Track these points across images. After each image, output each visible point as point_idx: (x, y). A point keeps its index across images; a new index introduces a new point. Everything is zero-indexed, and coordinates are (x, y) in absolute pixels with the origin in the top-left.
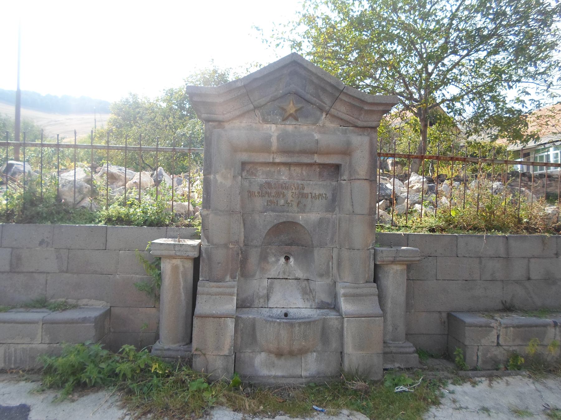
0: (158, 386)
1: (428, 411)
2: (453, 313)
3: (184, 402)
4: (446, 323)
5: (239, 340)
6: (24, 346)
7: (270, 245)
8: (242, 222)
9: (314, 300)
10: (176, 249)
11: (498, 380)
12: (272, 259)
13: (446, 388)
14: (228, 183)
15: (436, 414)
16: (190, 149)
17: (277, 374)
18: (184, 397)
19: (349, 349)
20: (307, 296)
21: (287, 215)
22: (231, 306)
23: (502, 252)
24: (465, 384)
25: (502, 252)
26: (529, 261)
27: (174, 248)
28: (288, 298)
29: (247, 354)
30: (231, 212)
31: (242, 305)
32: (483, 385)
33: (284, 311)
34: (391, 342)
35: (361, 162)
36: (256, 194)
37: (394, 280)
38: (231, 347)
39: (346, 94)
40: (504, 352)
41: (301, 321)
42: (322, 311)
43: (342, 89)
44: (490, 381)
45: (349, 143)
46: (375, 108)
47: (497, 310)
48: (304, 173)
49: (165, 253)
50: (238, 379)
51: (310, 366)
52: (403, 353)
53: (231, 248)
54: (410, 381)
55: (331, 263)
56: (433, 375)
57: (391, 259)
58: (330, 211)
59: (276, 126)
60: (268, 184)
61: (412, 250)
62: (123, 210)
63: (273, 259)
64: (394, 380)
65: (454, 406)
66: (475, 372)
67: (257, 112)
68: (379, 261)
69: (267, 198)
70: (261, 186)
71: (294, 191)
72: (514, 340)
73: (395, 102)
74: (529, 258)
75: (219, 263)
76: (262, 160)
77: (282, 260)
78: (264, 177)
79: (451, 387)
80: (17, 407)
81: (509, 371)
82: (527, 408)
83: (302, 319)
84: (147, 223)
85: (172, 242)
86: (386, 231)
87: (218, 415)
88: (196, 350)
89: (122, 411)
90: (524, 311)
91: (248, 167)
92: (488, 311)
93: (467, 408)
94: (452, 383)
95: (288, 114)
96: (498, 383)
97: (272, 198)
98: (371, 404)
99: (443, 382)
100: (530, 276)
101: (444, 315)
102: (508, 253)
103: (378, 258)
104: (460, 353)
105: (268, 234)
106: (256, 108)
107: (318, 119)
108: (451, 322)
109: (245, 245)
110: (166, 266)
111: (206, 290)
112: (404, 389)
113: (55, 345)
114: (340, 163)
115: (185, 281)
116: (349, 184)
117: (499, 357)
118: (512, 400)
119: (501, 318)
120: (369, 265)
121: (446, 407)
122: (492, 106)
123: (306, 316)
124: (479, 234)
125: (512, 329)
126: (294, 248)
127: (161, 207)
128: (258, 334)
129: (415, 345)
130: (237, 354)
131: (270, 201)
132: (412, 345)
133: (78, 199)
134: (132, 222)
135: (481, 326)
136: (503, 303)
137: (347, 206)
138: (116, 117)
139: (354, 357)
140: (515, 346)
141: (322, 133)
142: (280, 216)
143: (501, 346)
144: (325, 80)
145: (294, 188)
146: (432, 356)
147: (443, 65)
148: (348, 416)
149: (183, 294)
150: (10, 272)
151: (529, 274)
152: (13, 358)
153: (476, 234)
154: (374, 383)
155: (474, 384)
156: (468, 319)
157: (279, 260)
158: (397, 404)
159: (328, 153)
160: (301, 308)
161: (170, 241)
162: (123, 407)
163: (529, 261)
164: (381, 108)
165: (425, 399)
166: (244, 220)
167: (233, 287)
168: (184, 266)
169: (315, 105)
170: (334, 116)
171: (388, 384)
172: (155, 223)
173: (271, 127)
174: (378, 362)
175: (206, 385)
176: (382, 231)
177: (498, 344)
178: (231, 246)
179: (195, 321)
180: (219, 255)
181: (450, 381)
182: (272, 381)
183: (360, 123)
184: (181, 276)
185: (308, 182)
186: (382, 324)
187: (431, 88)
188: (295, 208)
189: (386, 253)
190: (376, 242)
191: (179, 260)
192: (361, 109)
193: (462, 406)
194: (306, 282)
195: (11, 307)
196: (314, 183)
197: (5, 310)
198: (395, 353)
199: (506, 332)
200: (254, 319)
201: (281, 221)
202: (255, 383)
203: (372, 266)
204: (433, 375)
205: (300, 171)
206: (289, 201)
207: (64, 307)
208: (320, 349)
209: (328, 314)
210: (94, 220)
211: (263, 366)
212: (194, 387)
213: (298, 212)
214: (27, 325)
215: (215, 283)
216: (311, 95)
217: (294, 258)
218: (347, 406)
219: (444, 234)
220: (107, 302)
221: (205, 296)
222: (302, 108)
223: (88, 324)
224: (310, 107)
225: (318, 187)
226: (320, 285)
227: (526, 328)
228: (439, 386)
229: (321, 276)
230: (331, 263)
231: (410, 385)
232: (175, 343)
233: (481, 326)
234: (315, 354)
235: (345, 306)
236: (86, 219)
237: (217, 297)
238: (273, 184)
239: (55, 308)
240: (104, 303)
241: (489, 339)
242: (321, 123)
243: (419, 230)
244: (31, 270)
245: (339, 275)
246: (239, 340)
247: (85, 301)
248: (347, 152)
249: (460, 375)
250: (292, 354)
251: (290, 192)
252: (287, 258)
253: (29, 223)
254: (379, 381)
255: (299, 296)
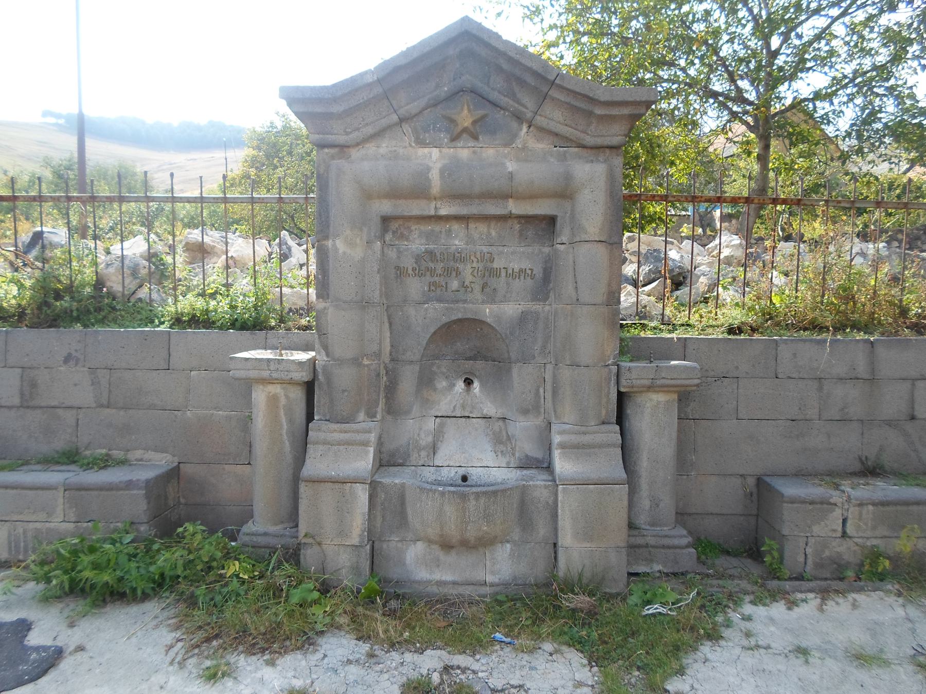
0: (238, 595)
1: (696, 649)
2: (768, 479)
3: (275, 622)
4: (755, 495)
5: (379, 519)
6: (38, 525)
7: (438, 358)
8: (386, 320)
9: (513, 455)
10: (272, 368)
11: (837, 599)
12: (442, 384)
13: (739, 610)
14: (358, 253)
15: (709, 656)
16: (306, 198)
17: (443, 578)
18: (276, 615)
19: (566, 538)
20: (502, 447)
21: (465, 308)
22: (364, 463)
23: (862, 369)
24: (775, 604)
25: (862, 369)
26: (913, 385)
27: (268, 366)
28: (467, 444)
29: (392, 544)
30: (363, 304)
31: (387, 460)
32: (809, 607)
33: (461, 471)
34: (648, 527)
35: (592, 210)
36: (410, 271)
37: (653, 420)
38: (363, 532)
39: (561, 88)
40: (856, 548)
41: (479, 489)
42: (525, 472)
43: (552, 78)
44: (823, 599)
45: (568, 177)
46: (615, 111)
47: (851, 474)
48: (493, 233)
49: (253, 374)
50: (373, 584)
51: (501, 566)
52: (669, 547)
53: (367, 366)
54: (672, 597)
55: (541, 390)
56: (719, 586)
57: (647, 382)
58: (539, 300)
59: (440, 152)
60: (431, 254)
61: (685, 367)
62: (200, 304)
63: (444, 384)
64: (645, 593)
65: (745, 643)
66: (797, 583)
67: (406, 127)
68: (624, 387)
69: (428, 278)
70: (418, 258)
71: (475, 265)
72: (874, 528)
73: (652, 99)
74: (914, 380)
75: (344, 391)
76: (416, 212)
77: (460, 385)
78: (423, 241)
79: (748, 609)
80: (12, 623)
81: (862, 583)
82: (881, 651)
83: (492, 485)
84: (238, 324)
85: (271, 357)
86: (649, 334)
87: (328, 646)
88: (306, 536)
89: (174, 634)
90: (899, 475)
91: (394, 225)
92: (833, 476)
93: (768, 647)
94: (751, 602)
95: (460, 128)
96: (837, 603)
97: (436, 279)
98: (595, 635)
99: (734, 599)
100: (916, 413)
101: (751, 481)
102: (873, 371)
103: (623, 382)
104: (773, 549)
105: (430, 341)
106: (402, 120)
107: (515, 136)
108: (762, 494)
109: (392, 360)
110: (260, 396)
111: (322, 436)
112: (661, 610)
113: (86, 524)
114: (554, 213)
115: (291, 421)
116: (571, 250)
117: (846, 557)
118: (858, 637)
119: (852, 488)
120: (609, 393)
121: (731, 644)
122: (890, 106)
123: (499, 480)
124: (819, 338)
125: (871, 507)
126: (480, 364)
127: (261, 297)
128: (409, 511)
129: (690, 533)
130: (376, 543)
131: (434, 284)
132: (685, 532)
133: (133, 287)
134: (214, 323)
135: (812, 503)
136: (860, 459)
137: (568, 290)
138: (255, 152)
139: (576, 552)
140: (876, 537)
141: (519, 160)
142: (452, 309)
143: (850, 537)
144: (521, 64)
145: (475, 260)
146: (728, 553)
147: (799, 37)
148: (551, 655)
149: (287, 443)
150: (21, 406)
151: (913, 408)
152: (22, 544)
153: (815, 337)
154: (609, 597)
155: (792, 604)
156: (790, 489)
157: (454, 385)
158: (641, 638)
159: (532, 196)
160: (490, 466)
161: (267, 354)
162: (177, 628)
163: (913, 385)
164: (626, 111)
165: (693, 629)
166: (389, 317)
167: (370, 432)
168: (287, 397)
169: (508, 111)
170: (541, 129)
171: (633, 600)
172: (252, 325)
173: (430, 154)
174: (618, 564)
175: (316, 595)
176: (642, 334)
177: (844, 535)
178: (366, 362)
179: (303, 488)
180: (345, 377)
181: (747, 598)
182: (435, 589)
183: (589, 140)
184: (282, 413)
185: (501, 248)
186: (626, 498)
187: (774, 80)
188: (478, 295)
189: (637, 372)
190: (622, 353)
191: (279, 386)
192: (590, 114)
193: (760, 643)
194: (501, 423)
195: (22, 463)
196: (511, 250)
197: (11, 468)
198: (653, 547)
199: (860, 514)
200: (403, 485)
201: (454, 318)
202: (405, 593)
203: (614, 396)
204: (719, 586)
205: (485, 230)
206: (467, 283)
207: (105, 463)
208: (517, 539)
209: (532, 479)
210: (152, 322)
211: (420, 564)
212: (296, 596)
213: (483, 302)
214: (40, 492)
215: (339, 425)
216: (499, 92)
217: (481, 382)
218: (554, 636)
219: (756, 336)
220: (174, 456)
221: (321, 447)
222: (483, 117)
223: (135, 492)
224: (499, 115)
225: (517, 257)
226: (523, 428)
227: (899, 508)
228: (725, 606)
229: (525, 412)
230: (541, 390)
231: (673, 604)
232: (277, 525)
233: (812, 503)
234: (508, 545)
235: (562, 465)
236: (141, 320)
237: (342, 448)
238: (438, 254)
239: (89, 464)
240: (169, 457)
241: (827, 526)
242: (519, 143)
243: (710, 330)
244: (53, 404)
245: (555, 411)
246: (379, 519)
247: (138, 454)
248: (565, 192)
249: (769, 587)
250: (466, 545)
251: (469, 266)
252: (468, 382)
253: (50, 327)
254: (618, 594)
255: (488, 447)
